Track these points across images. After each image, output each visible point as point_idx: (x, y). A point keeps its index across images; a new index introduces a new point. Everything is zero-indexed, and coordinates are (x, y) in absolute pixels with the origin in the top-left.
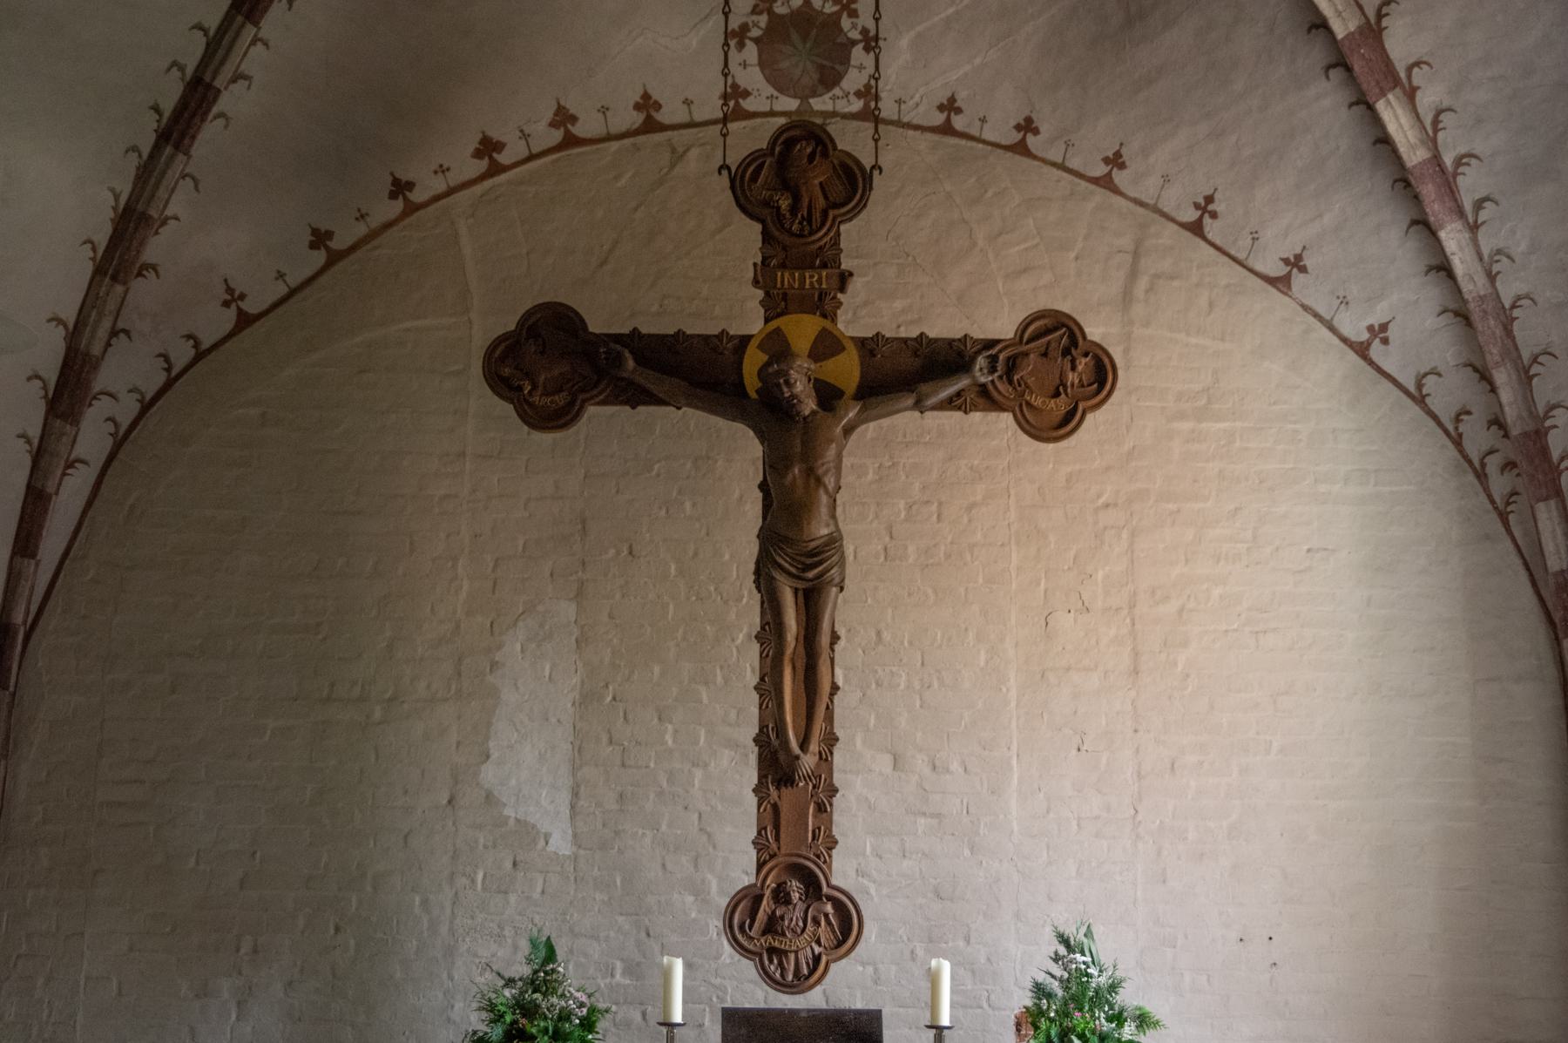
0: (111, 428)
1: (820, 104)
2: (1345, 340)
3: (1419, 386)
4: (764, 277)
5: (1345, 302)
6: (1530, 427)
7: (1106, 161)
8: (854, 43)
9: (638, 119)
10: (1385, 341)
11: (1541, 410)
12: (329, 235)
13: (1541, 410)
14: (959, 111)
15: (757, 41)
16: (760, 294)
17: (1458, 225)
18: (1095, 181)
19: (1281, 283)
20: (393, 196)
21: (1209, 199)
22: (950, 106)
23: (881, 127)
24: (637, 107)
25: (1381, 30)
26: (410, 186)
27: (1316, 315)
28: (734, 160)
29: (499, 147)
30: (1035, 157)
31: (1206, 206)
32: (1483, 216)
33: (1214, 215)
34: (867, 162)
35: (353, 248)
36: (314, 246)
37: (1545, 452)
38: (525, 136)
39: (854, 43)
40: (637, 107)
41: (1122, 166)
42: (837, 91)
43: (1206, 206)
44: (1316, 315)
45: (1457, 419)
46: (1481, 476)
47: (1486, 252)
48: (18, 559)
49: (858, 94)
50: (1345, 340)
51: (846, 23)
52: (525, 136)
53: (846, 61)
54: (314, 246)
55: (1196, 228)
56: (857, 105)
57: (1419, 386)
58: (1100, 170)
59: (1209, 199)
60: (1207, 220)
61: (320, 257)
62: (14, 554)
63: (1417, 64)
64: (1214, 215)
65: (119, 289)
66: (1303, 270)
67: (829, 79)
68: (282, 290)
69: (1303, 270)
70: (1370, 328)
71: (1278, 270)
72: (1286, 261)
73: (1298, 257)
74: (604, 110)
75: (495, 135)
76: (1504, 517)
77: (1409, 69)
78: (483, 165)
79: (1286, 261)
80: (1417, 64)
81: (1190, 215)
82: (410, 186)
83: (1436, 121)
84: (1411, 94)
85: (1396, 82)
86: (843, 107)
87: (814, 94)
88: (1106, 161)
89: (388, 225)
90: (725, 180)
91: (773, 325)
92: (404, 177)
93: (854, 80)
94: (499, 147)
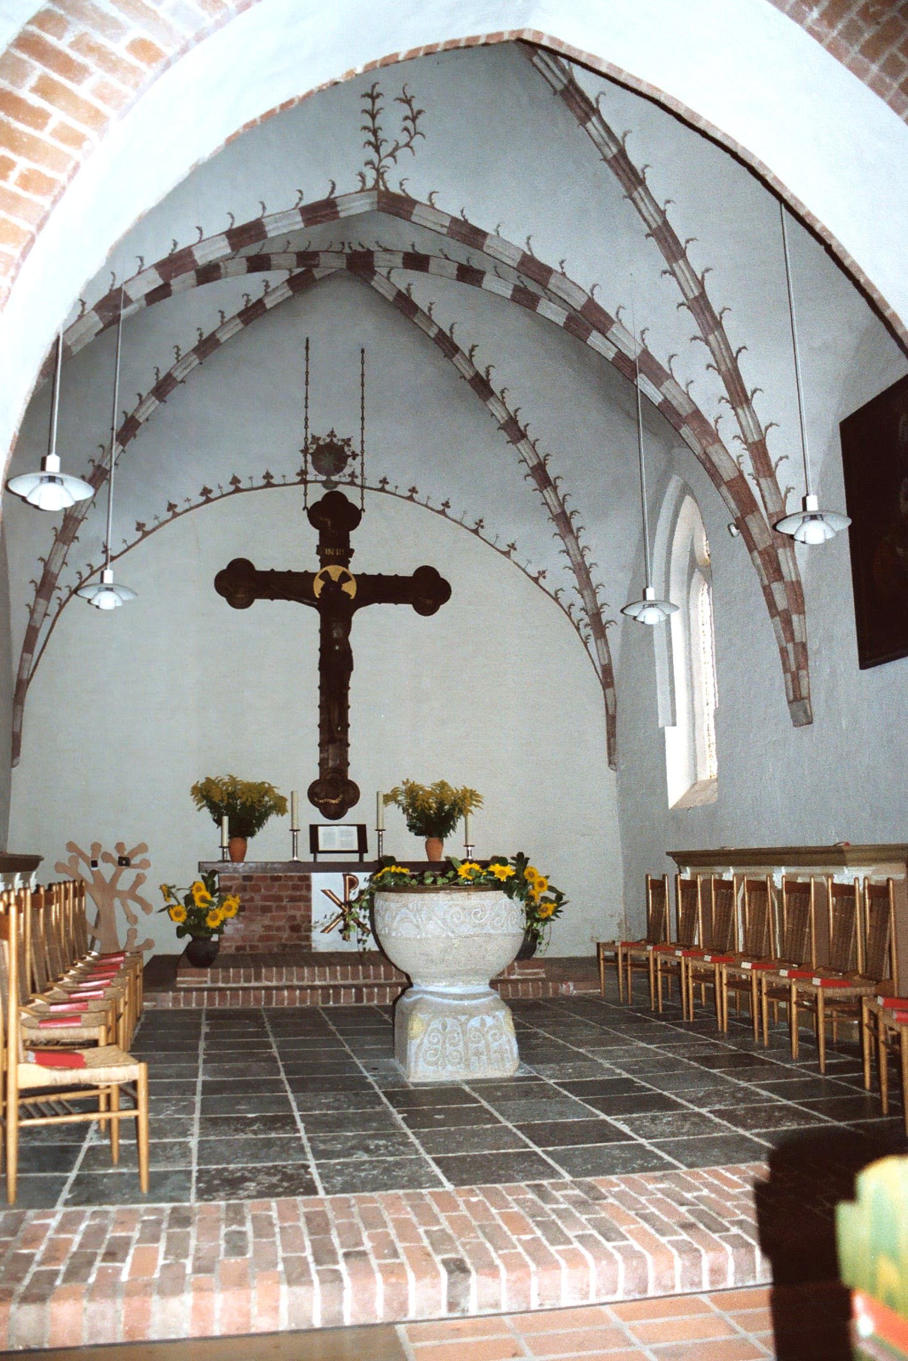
0: (58, 601)
1: (335, 478)
2: (529, 576)
3: (556, 594)
4: (320, 550)
5: (529, 562)
6: (595, 611)
7: (443, 505)
8: (349, 456)
9: (264, 482)
10: (544, 577)
11: (599, 605)
12: (144, 525)
13: (599, 605)
14: (388, 483)
15: (311, 454)
16: (319, 557)
17: (571, 537)
18: (438, 512)
19: (507, 554)
20: (169, 510)
21: (481, 521)
22: (384, 481)
23: (365, 490)
24: (264, 477)
25: (545, 464)
26: (175, 506)
27: (519, 566)
28: (309, 506)
29: (210, 491)
30: (587, 648)
31: (480, 524)
32: (580, 534)
33: (482, 527)
34: (360, 507)
35: (154, 530)
36: (138, 529)
37: (600, 620)
38: (220, 487)
39: (349, 456)
40: (264, 477)
41: (449, 507)
42: (341, 474)
43: (480, 524)
44: (519, 566)
45: (569, 607)
46: (578, 629)
47: (581, 547)
48: (25, 655)
49: (349, 475)
50: (529, 576)
51: (346, 449)
52: (220, 487)
53: (345, 463)
54: (138, 529)
55: (476, 532)
56: (349, 479)
57: (556, 594)
58: (441, 508)
59: (481, 521)
60: (480, 529)
61: (140, 534)
62: (23, 652)
63: (558, 477)
64: (482, 527)
65: (66, 547)
66: (515, 549)
67: (339, 469)
68: (125, 547)
69: (515, 549)
70: (539, 572)
71: (506, 549)
72: (509, 546)
73: (513, 544)
74: (251, 478)
75: (209, 487)
76: (586, 644)
77: (555, 479)
78: (204, 498)
79: (509, 546)
80: (558, 477)
81: (474, 527)
82: (175, 506)
83: (564, 499)
84: (555, 488)
85: (550, 484)
86: (344, 480)
87: (333, 475)
88: (443, 505)
89: (167, 521)
90: (305, 512)
91: (324, 569)
92: (173, 503)
93: (347, 470)
94: (210, 491)
